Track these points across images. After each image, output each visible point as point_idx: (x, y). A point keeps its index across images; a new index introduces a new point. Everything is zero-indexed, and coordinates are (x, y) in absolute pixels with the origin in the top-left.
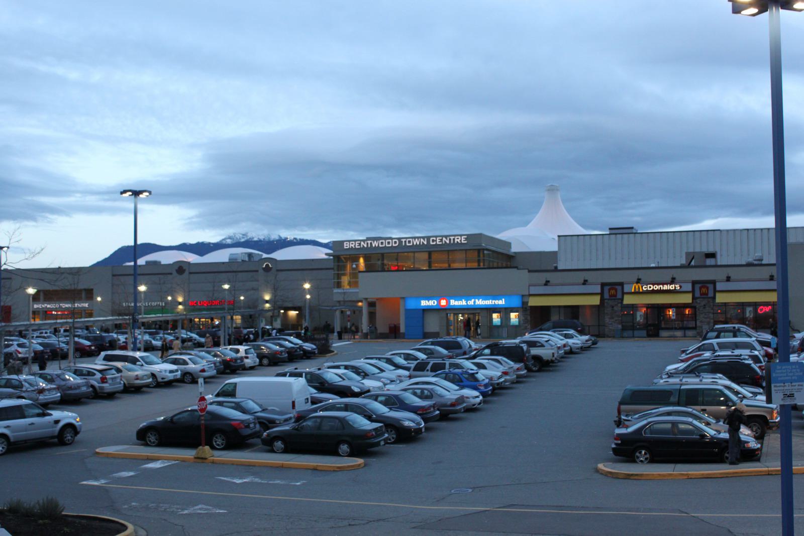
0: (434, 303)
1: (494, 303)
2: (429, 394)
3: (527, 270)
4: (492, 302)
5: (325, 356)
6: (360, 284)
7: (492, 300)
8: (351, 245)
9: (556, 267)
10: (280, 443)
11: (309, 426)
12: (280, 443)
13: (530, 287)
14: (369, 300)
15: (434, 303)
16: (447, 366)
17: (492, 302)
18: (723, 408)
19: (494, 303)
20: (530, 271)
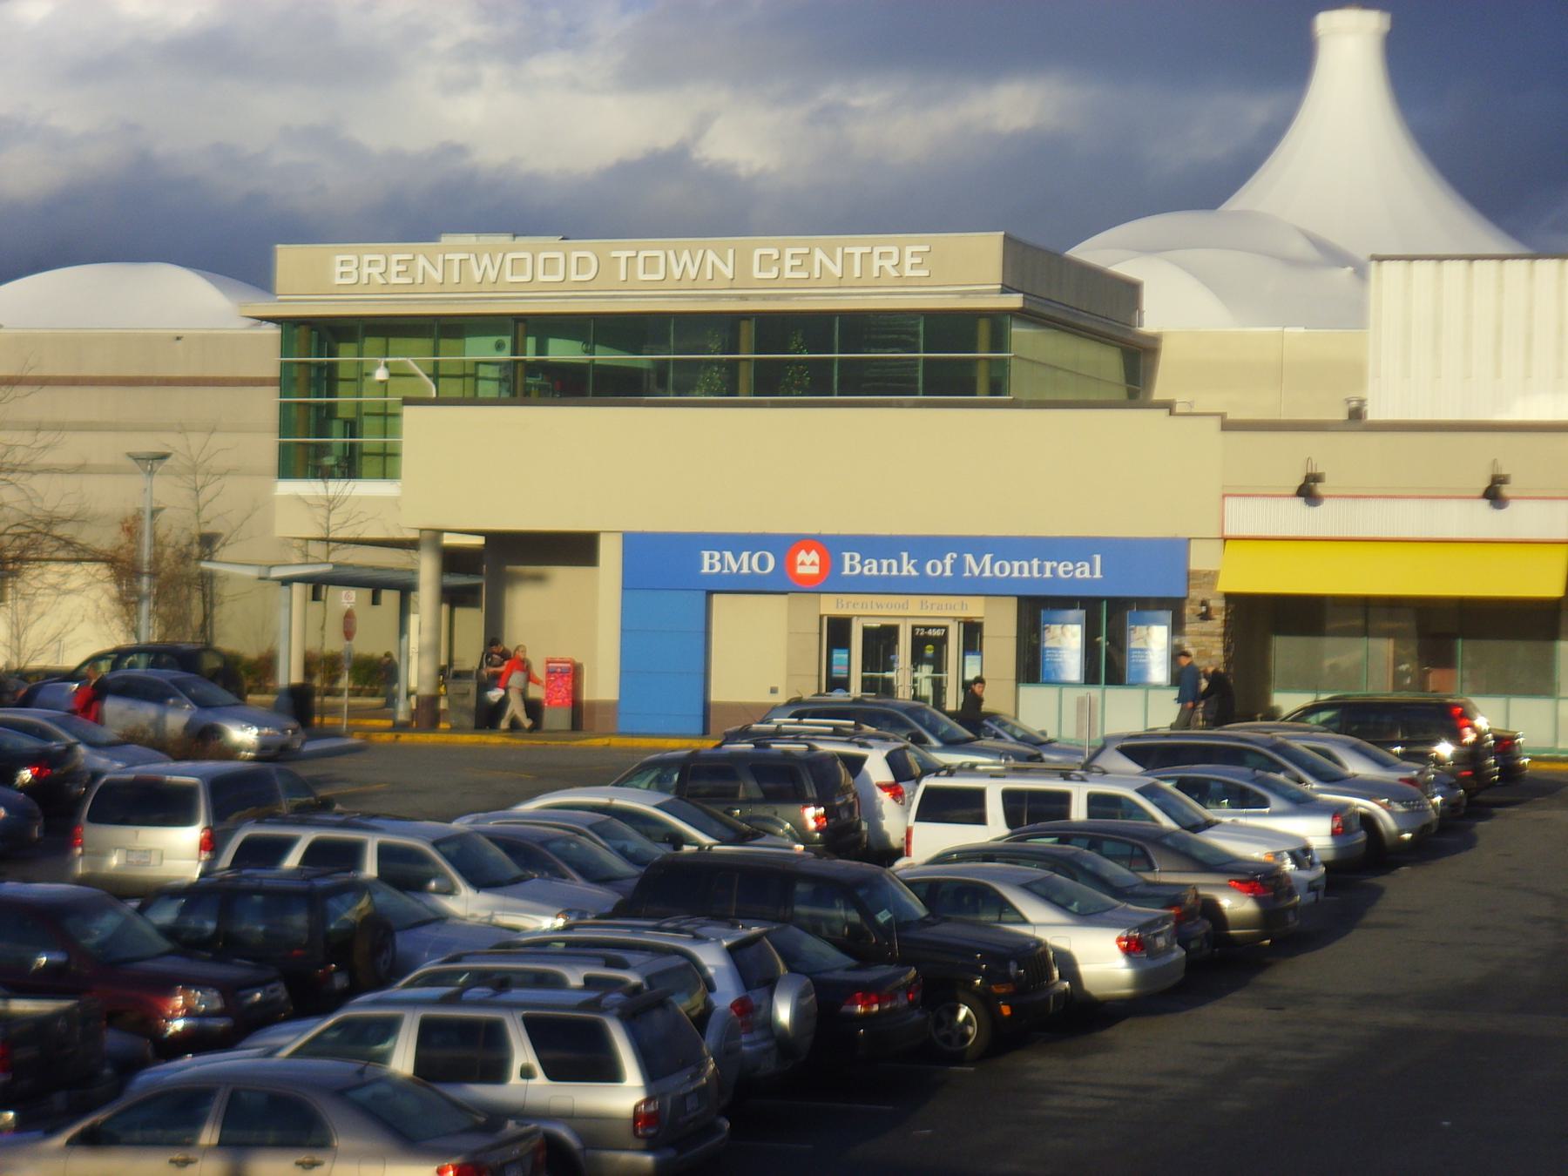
0: (763, 563)
1: (1053, 570)
2: (1263, 875)
3: (1215, 423)
4: (1041, 569)
5: (336, 565)
6: (409, 459)
7: (1042, 559)
8: (366, 270)
9: (1356, 415)
10: (814, 556)
11: (1285, 864)
12: (814, 556)
13: (1229, 502)
14: (449, 540)
15: (763, 563)
16: (994, 807)
17: (1041, 569)
18: (928, 1131)
19: (1053, 570)
20: (1228, 426)
